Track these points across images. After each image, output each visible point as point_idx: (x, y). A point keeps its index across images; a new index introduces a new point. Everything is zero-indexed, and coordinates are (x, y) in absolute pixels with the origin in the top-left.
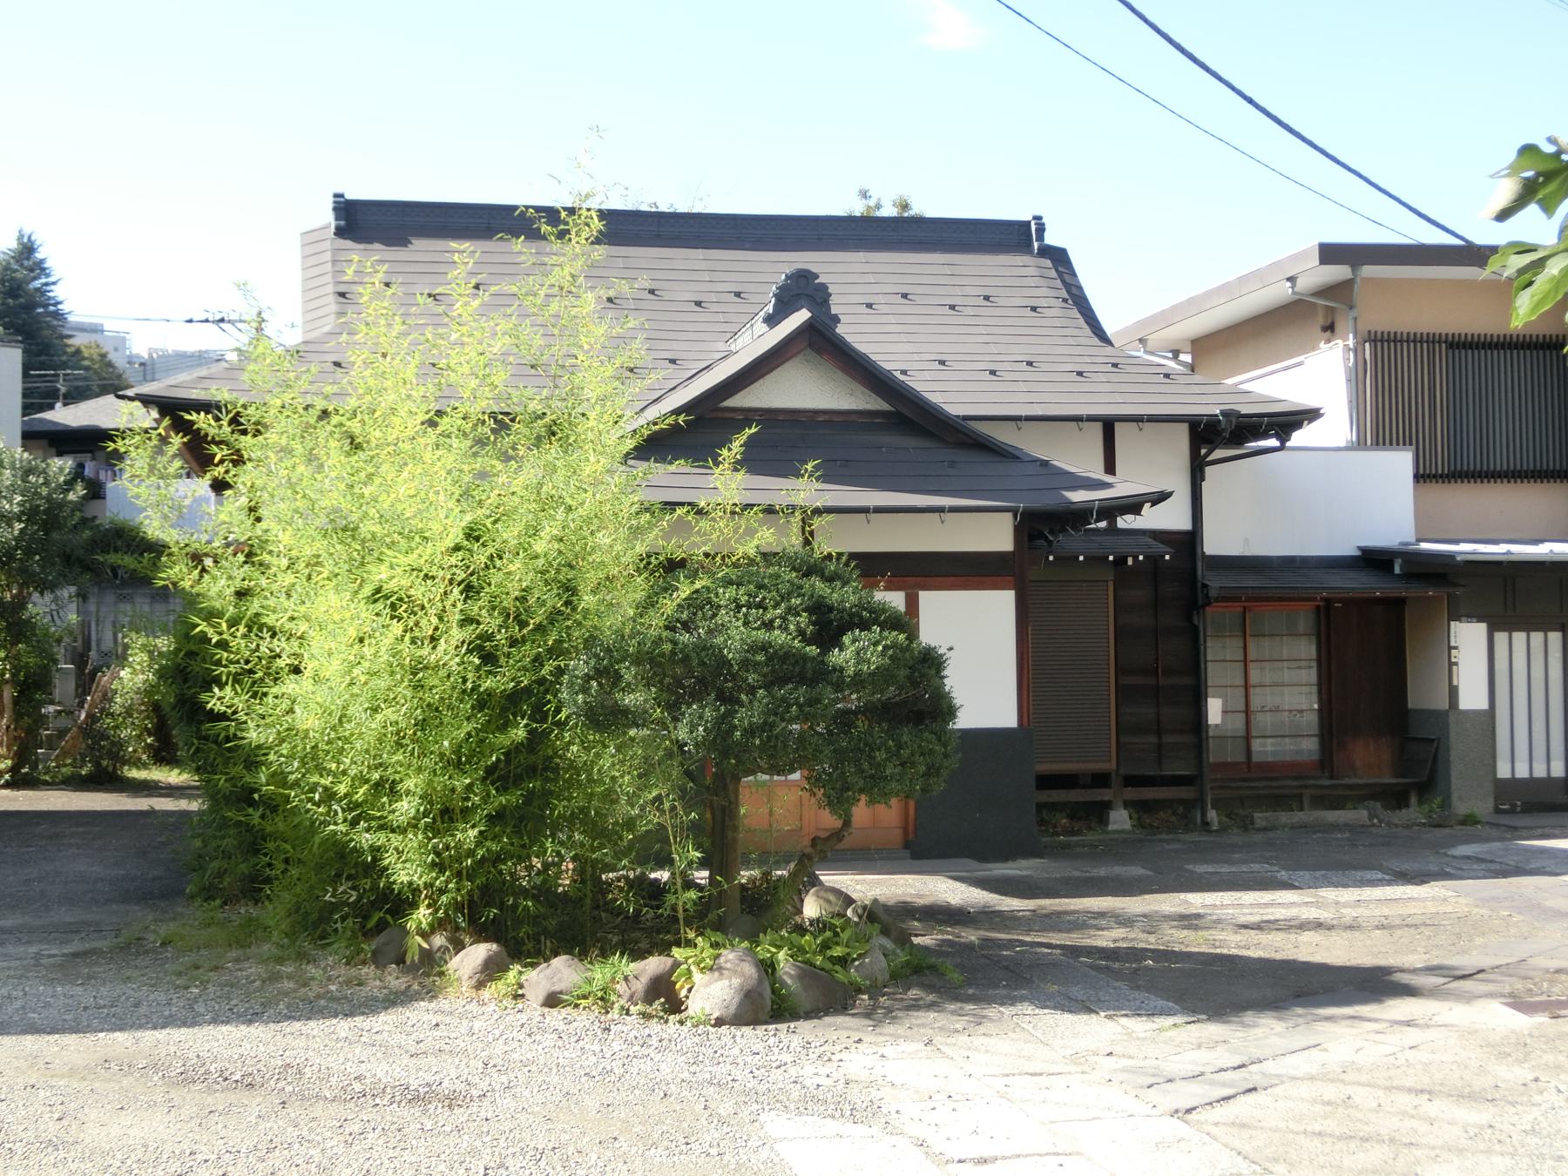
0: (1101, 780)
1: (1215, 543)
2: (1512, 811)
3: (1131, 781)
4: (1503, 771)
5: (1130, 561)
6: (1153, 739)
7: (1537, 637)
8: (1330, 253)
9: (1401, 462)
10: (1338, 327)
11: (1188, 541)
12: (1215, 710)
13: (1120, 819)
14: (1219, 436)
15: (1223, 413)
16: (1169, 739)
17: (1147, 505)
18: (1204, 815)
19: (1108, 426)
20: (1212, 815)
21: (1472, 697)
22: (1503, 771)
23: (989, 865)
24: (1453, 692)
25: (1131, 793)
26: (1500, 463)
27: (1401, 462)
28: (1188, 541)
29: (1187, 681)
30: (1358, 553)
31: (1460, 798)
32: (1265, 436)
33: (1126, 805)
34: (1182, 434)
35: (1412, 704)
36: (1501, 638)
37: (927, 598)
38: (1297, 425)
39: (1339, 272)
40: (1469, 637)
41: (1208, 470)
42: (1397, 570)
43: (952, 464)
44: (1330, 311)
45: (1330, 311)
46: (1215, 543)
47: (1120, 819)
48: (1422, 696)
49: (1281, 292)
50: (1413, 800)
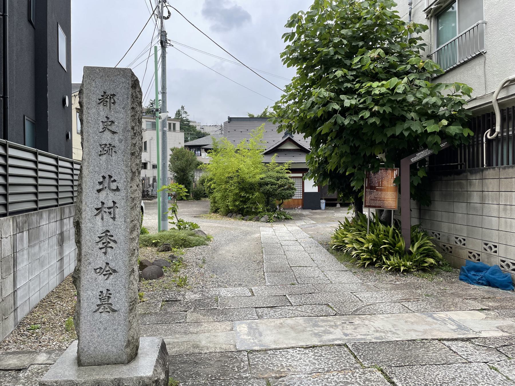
0: (336, 200)
13: (338, 205)
47: (338, 205)
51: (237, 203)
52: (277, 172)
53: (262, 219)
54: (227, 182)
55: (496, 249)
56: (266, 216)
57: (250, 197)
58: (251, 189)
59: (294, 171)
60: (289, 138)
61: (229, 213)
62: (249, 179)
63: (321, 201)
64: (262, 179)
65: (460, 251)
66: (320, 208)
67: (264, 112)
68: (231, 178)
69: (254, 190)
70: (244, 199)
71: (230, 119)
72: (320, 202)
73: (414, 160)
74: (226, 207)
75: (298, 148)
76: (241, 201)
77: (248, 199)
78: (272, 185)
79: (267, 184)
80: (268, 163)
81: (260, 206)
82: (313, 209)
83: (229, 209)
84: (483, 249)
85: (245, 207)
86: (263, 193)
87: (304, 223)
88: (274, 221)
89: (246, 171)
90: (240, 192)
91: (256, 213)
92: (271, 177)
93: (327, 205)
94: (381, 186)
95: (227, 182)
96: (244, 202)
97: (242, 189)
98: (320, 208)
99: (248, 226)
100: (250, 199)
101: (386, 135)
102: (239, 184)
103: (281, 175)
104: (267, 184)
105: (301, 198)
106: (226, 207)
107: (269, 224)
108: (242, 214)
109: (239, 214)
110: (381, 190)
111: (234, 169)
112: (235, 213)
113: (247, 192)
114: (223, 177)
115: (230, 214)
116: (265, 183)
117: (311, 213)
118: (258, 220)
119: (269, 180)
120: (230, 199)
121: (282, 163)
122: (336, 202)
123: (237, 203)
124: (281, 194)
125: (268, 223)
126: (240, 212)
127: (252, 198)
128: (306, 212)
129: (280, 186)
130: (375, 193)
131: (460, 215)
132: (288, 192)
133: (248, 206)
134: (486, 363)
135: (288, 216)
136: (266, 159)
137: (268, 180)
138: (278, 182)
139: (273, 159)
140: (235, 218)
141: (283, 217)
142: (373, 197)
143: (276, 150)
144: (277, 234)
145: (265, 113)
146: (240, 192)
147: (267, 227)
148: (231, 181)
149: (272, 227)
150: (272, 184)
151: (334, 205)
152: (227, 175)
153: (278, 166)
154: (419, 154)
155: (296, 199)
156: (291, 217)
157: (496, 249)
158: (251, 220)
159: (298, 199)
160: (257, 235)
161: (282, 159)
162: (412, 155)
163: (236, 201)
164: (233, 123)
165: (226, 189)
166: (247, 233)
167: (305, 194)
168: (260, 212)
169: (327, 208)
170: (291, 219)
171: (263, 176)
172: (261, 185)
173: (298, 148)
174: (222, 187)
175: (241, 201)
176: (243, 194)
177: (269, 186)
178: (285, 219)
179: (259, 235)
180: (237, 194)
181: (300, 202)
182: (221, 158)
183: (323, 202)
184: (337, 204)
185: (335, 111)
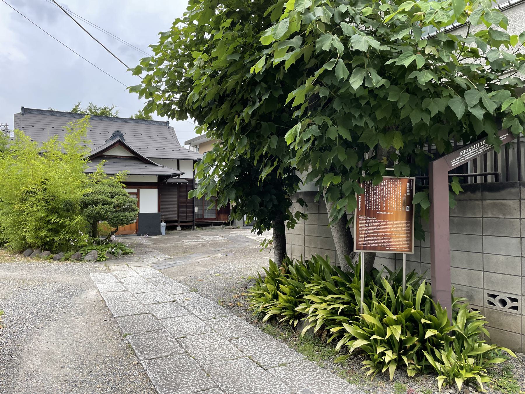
0: (176, 221)
3: (181, 222)
12: (196, 209)
13: (179, 228)
19: (178, 160)
20: (195, 227)
25: (181, 224)
33: (180, 226)
47: (179, 228)
51: (43, 233)
52: (109, 186)
53: (88, 257)
54: (23, 200)
55: (515, 304)
56: (93, 251)
57: (67, 223)
58: (68, 211)
59: (130, 185)
60: (119, 141)
61: (25, 249)
62: (64, 195)
63: (162, 224)
64: (87, 195)
65: (503, 318)
66: (160, 233)
67: (74, 109)
68: (31, 193)
69: (74, 211)
70: (54, 227)
71: (25, 111)
72: (160, 225)
73: (456, 162)
74: (21, 239)
76: (49, 230)
77: (63, 226)
78: (103, 205)
79: (96, 203)
80: (91, 173)
81: (85, 238)
83: (26, 243)
84: (487, 303)
85: (57, 239)
86: (88, 216)
87: (155, 260)
88: (107, 259)
89: (61, 182)
90: (47, 216)
91: (77, 248)
92: (101, 192)
93: (168, 228)
94: (386, 211)
95: (23, 200)
96: (55, 231)
97: (52, 211)
98: (160, 233)
99: (66, 272)
100: (66, 226)
101: (428, 111)
102: (47, 202)
103: (117, 190)
104: (96, 203)
106: (21, 239)
107: (100, 266)
108: (50, 250)
109: (45, 250)
110: (385, 217)
111: (38, 180)
112: (38, 248)
113: (60, 216)
114: (15, 192)
115: (28, 251)
116: (92, 201)
117: (150, 240)
118: (80, 259)
119: (99, 197)
120: (30, 227)
121: (113, 174)
122: (176, 224)
123: (43, 233)
124: (117, 217)
125: (98, 264)
126: (47, 247)
127: (69, 225)
128: (144, 239)
130: (375, 225)
131: (502, 258)
133: (62, 237)
135: (127, 250)
136: (89, 167)
137: (96, 197)
138: (113, 200)
139: (100, 167)
140: (38, 257)
141: (120, 252)
142: (371, 232)
143: (96, 157)
144: (128, 287)
145: (75, 110)
146: (47, 216)
147: (100, 271)
148: (30, 199)
149: (109, 271)
151: (174, 228)
152: (24, 188)
153: (107, 178)
154: (464, 151)
156: (132, 251)
157: (515, 304)
158: (67, 259)
160: (92, 294)
161: (111, 169)
162: (452, 154)
163: (39, 229)
165: (21, 212)
166: (72, 292)
168: (82, 246)
169: (170, 232)
170: (132, 253)
171: (89, 190)
172: (85, 205)
174: (13, 208)
175: (49, 230)
176: (53, 219)
177: (100, 206)
178: (123, 254)
179: (95, 292)
180: (42, 218)
182: (13, 161)
183: (163, 224)
184: (177, 226)
185: (333, 53)
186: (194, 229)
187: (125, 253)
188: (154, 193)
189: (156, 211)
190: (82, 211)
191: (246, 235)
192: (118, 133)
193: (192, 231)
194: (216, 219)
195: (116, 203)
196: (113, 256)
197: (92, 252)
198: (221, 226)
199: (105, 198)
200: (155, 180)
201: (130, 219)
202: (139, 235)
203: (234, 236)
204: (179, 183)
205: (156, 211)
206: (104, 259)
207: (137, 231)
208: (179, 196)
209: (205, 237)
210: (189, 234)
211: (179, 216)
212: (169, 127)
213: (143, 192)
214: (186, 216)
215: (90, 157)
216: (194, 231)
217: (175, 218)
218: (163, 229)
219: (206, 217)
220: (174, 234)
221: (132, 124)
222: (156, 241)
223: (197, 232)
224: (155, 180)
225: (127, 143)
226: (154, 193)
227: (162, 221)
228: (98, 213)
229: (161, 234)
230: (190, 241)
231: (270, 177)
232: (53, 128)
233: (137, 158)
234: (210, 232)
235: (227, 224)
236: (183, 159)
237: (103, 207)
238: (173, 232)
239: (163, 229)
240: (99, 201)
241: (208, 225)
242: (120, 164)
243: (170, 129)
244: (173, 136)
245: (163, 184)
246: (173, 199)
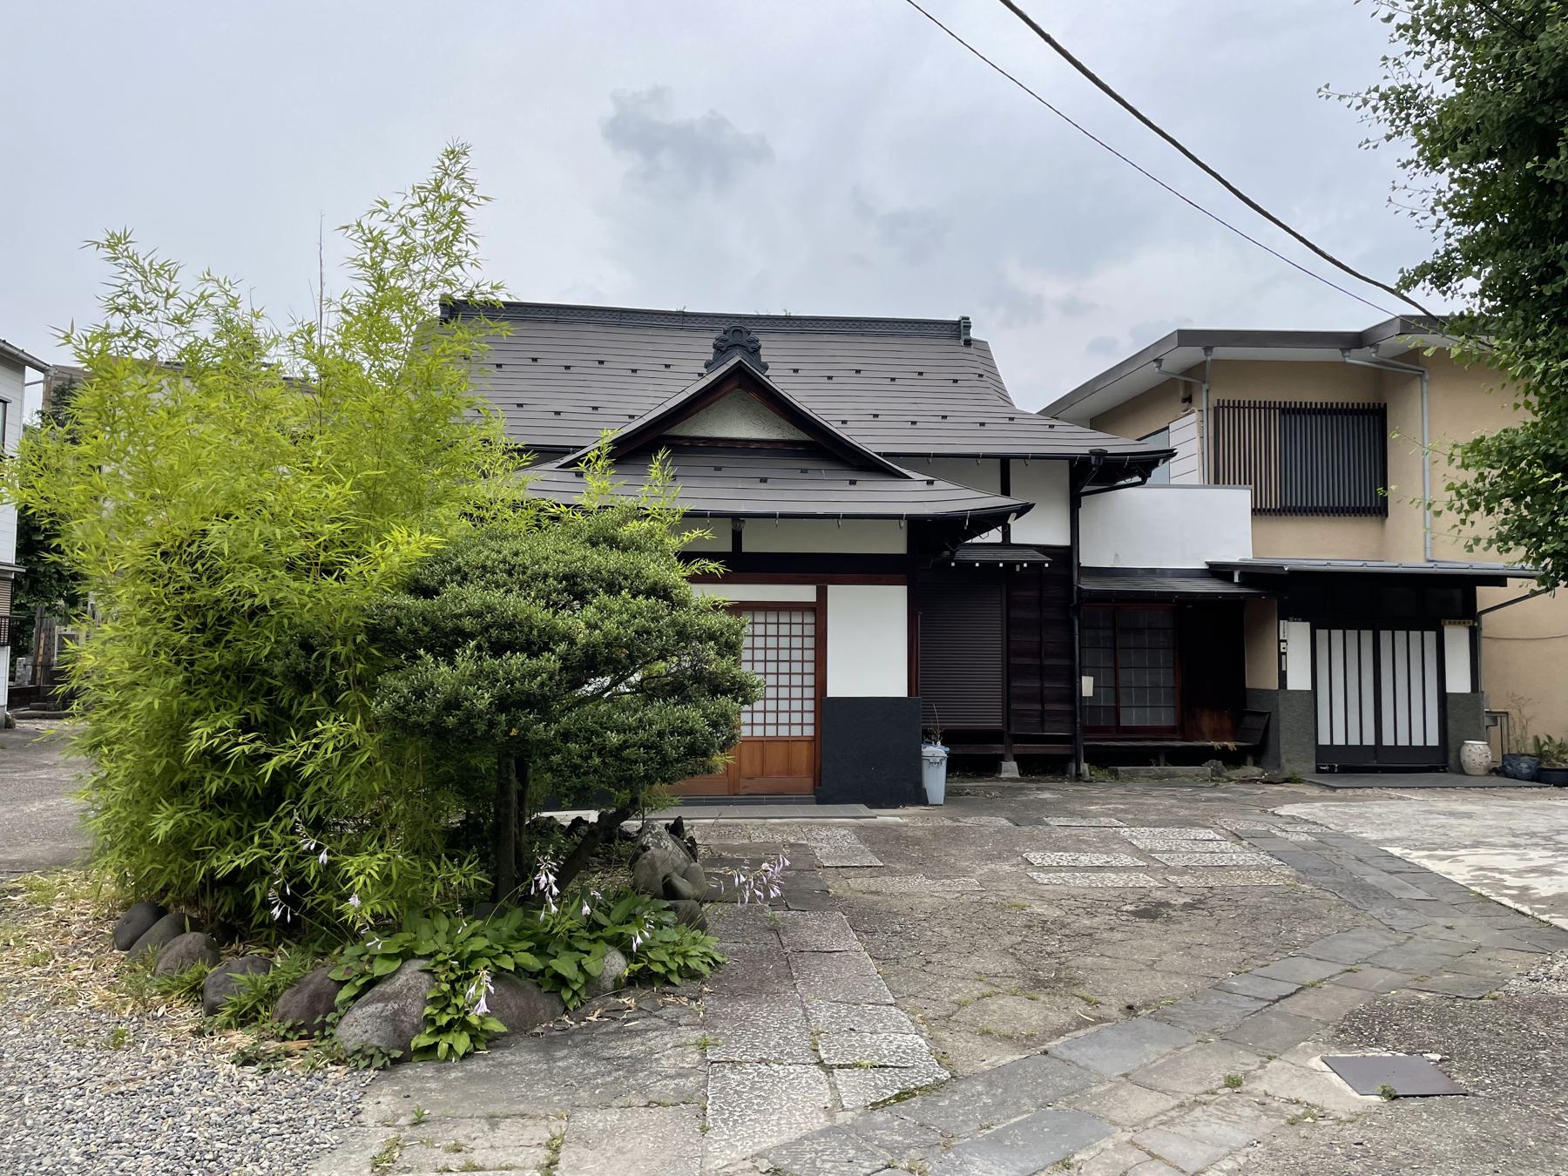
0: (994, 736)
1: (1087, 559)
2: (1331, 770)
3: (1018, 739)
4: (1324, 740)
5: (1018, 568)
6: (1039, 707)
7: (1403, 741)
8: (1186, 337)
9: (1240, 499)
10: (1195, 398)
11: (1065, 556)
12: (1087, 685)
13: (1010, 769)
14: (1095, 475)
15: (1092, 453)
16: (1049, 707)
17: (1013, 515)
18: (1078, 768)
19: (1005, 461)
20: (1085, 767)
21: (1299, 679)
22: (1324, 740)
23: (875, 812)
24: (1283, 676)
25: (1019, 748)
26: (1322, 502)
27: (1240, 499)
28: (1065, 556)
29: (1066, 662)
30: (1205, 567)
31: (1288, 760)
32: (1131, 476)
33: (1017, 758)
34: (1063, 474)
35: (1249, 684)
36: (1322, 634)
37: (832, 590)
38: (1155, 464)
39: (1194, 354)
40: (1296, 636)
41: (1083, 499)
42: (1236, 579)
43: (853, 482)
44: (1188, 386)
45: (1188, 386)
46: (1089, 557)
47: (1010, 769)
48: (1261, 677)
49: (1150, 374)
50: (1250, 759)
60: (739, 369)
72: (919, 758)
75: (801, 436)
78: (498, 649)
82: (876, 801)
93: (955, 766)
104: (445, 642)
105: (809, 731)
122: (998, 749)
129: (589, 662)
132: (665, 713)
134: (1151, 966)
141: (617, 965)
150: (505, 637)
151: (989, 767)
155: (777, 740)
159: (789, 741)
164: (461, 331)
167: (831, 712)
169: (969, 785)
172: (388, 641)
173: (801, 436)
177: (465, 661)
181: (803, 755)
183: (936, 751)
184: (1002, 758)
186: (1078, 777)
187: (642, 979)
188: (891, 602)
189: (902, 692)
190: (366, 684)
191: (1370, 834)
192: (737, 339)
193: (1071, 788)
194: (1180, 730)
195: (581, 639)
196: (544, 1004)
197: (401, 980)
198: (1207, 769)
199: (513, 603)
200: (895, 544)
201: (672, 746)
202: (822, 800)
203: (1299, 836)
204: (1010, 565)
205: (902, 692)
206: (462, 1043)
207: (818, 779)
208: (1011, 626)
209: (1144, 837)
210: (1057, 809)
211: (1008, 714)
212: (968, 343)
213: (841, 597)
214: (1042, 713)
215: (619, 443)
216: (1082, 787)
217: (995, 722)
218: (935, 780)
219: (1131, 718)
220: (991, 807)
221: (825, 338)
222: (889, 845)
223: (1094, 791)
224: (895, 544)
225: (778, 379)
226: (891, 602)
227: (928, 737)
228: (452, 704)
229: (925, 802)
230: (1066, 858)
231: (565, 802)
232: (535, 360)
233: (823, 449)
234: (1160, 799)
235: (1233, 759)
236: (1024, 457)
237: (489, 662)
238: (983, 784)
239: (935, 780)
240: (467, 623)
241: (1141, 758)
242: (740, 473)
243: (971, 350)
244: (987, 372)
245: (933, 566)
246: (984, 642)
